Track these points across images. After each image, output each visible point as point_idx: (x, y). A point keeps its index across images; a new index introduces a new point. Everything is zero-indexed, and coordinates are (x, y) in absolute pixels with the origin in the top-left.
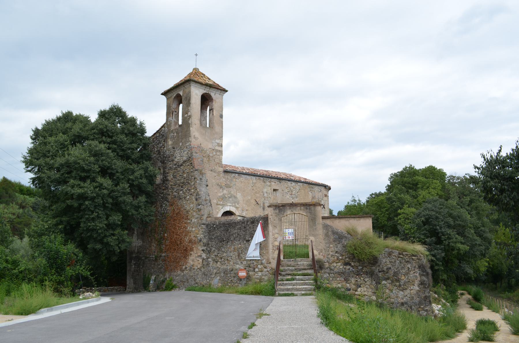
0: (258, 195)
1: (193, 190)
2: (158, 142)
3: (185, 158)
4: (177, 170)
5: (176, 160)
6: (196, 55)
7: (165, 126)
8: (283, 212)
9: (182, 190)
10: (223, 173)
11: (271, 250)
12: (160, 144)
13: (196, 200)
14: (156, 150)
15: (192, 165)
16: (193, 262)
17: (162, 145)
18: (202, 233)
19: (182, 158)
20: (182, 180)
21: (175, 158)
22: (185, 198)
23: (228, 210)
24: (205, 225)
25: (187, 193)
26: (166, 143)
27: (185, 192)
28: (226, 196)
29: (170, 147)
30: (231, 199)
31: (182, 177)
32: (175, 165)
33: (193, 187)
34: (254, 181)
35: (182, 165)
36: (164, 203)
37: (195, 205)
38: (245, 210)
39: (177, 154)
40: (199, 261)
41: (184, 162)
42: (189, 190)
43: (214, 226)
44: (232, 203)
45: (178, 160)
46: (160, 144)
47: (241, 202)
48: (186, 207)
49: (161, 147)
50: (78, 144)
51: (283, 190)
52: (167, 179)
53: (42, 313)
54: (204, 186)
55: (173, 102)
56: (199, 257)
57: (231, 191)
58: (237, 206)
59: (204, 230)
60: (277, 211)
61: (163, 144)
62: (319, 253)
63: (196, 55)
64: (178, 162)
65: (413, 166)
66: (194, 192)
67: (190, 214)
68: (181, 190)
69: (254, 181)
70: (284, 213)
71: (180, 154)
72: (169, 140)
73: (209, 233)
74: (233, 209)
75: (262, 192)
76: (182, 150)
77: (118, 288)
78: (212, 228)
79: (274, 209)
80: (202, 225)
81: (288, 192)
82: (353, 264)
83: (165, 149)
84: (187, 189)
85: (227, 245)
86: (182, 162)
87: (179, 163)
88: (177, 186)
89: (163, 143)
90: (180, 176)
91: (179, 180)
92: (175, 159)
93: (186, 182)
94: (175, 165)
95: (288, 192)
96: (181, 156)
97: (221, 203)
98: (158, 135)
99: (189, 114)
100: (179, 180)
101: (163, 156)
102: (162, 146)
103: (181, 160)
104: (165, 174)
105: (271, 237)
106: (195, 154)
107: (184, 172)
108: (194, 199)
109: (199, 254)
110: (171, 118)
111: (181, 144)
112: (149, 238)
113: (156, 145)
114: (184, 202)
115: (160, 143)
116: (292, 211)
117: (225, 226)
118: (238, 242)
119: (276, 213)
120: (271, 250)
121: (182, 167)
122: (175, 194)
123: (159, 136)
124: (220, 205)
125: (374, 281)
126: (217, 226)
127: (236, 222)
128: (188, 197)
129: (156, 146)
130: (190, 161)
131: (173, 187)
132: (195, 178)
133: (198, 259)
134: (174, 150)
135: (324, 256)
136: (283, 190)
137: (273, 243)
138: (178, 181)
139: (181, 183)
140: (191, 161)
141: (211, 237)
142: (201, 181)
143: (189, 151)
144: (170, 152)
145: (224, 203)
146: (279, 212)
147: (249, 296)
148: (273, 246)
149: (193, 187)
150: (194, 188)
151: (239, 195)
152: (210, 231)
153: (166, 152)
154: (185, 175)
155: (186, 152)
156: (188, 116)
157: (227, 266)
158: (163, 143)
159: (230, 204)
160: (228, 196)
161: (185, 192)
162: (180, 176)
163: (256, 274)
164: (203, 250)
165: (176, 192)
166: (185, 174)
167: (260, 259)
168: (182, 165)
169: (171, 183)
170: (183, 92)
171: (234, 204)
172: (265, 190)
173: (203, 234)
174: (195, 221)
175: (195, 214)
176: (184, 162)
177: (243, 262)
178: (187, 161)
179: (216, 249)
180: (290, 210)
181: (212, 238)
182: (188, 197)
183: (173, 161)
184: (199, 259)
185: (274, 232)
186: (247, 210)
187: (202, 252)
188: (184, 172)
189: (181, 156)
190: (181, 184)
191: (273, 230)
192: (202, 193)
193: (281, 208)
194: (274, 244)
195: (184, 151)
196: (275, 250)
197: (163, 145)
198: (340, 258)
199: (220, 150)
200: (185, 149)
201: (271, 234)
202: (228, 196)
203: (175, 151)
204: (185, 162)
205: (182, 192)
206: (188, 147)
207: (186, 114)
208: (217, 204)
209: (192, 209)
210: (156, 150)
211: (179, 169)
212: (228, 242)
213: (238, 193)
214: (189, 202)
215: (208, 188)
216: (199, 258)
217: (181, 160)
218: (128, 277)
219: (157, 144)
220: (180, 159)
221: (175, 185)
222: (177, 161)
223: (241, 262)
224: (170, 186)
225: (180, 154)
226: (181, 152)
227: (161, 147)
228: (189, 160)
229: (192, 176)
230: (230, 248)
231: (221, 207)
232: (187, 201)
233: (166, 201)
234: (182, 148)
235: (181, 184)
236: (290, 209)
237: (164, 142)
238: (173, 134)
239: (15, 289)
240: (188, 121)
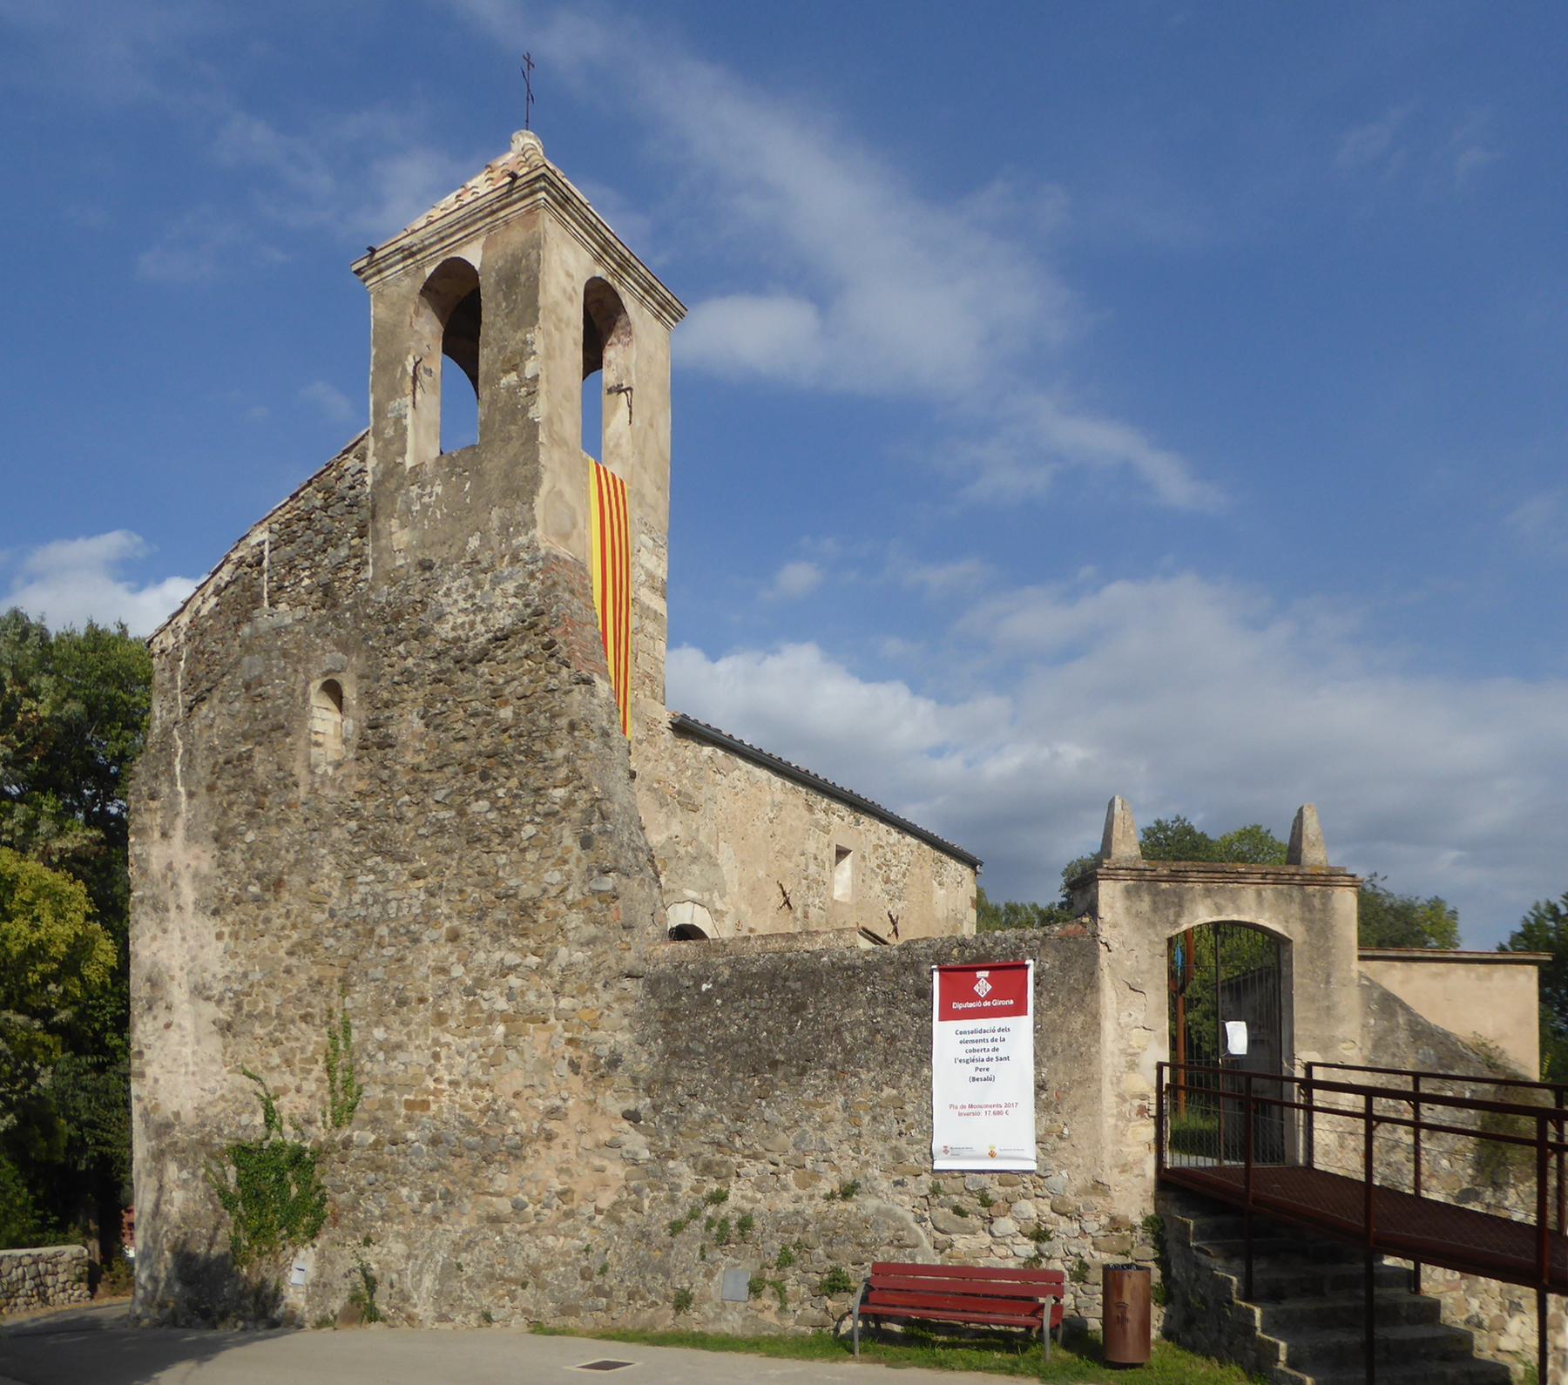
1: (559, 793)
2: (319, 539)
3: (503, 619)
4: (449, 683)
5: (445, 630)
7: (365, 448)
8: (1171, 912)
9: (488, 791)
10: (668, 734)
11: (1112, 1121)
12: (336, 546)
13: (586, 843)
15: (552, 656)
16: (565, 1178)
17: (344, 552)
18: (626, 1022)
19: (483, 621)
20: (486, 740)
21: (440, 617)
22: (507, 834)
24: (641, 982)
25: (523, 806)
26: (376, 538)
27: (508, 801)
28: (682, 851)
29: (400, 562)
30: (695, 869)
31: (486, 724)
32: (437, 657)
33: (563, 772)
34: (779, 797)
35: (483, 656)
36: (369, 863)
37: (576, 873)
39: (446, 595)
40: (601, 1170)
41: (501, 638)
42: (537, 791)
43: (705, 987)
44: (701, 890)
45: (453, 629)
46: (336, 546)
47: (733, 888)
48: (513, 882)
49: (338, 568)
51: (863, 857)
52: (387, 736)
55: (417, 313)
56: (607, 1152)
57: (698, 829)
58: (719, 906)
59: (630, 1007)
60: (1145, 905)
61: (351, 547)
64: (457, 640)
65: (1264, 829)
66: (570, 803)
67: (542, 919)
68: (478, 795)
69: (779, 797)
70: (1179, 915)
71: (472, 596)
72: (394, 522)
73: (665, 1023)
74: (702, 920)
75: (803, 854)
76: (485, 571)
77: (718, 1318)
78: (690, 997)
79: (1128, 892)
80: (627, 983)
83: (369, 572)
85: (796, 1087)
86: (482, 639)
87: (462, 649)
88: (449, 771)
89: (355, 542)
90: (475, 715)
91: (464, 739)
92: (437, 628)
93: (515, 749)
94: (437, 657)
96: (481, 609)
98: (318, 503)
99: (530, 368)
100: (464, 739)
101: (355, 615)
102: (348, 558)
103: (480, 628)
104: (514, 646)
107: (496, 694)
108: (569, 840)
109: (606, 1136)
110: (409, 400)
112: (274, 1051)
113: (307, 558)
114: (503, 859)
115: (331, 541)
116: (1219, 910)
117: (779, 983)
118: (884, 1075)
119: (1137, 915)
120: (1112, 1121)
121: (483, 668)
122: (445, 814)
123: (325, 508)
126: (720, 987)
127: (859, 962)
128: (529, 830)
129: (307, 564)
130: (543, 634)
131: (427, 777)
132: (572, 727)
133: (597, 1162)
134: (427, 575)
136: (863, 857)
137: (1119, 1080)
138: (459, 746)
139: (480, 754)
140: (546, 629)
141: (681, 1044)
143: (532, 575)
144: (406, 590)
146: (1155, 908)
147: (650, 1348)
148: (1122, 1098)
150: (567, 781)
151: (726, 855)
152: (671, 1011)
153: (371, 588)
154: (506, 713)
155: (510, 587)
156: (522, 382)
157: (798, 1199)
158: (355, 542)
160: (687, 852)
161: (508, 801)
162: (475, 715)
163: (1001, 1251)
164: (632, 1116)
165: (448, 807)
166: (506, 703)
167: (1033, 1166)
168: (483, 656)
169: (410, 758)
170: (485, 247)
173: (631, 1028)
174: (579, 956)
175: (575, 919)
176: (497, 639)
177: (909, 1179)
178: (516, 633)
179: (720, 1109)
180: (1208, 902)
181: (688, 1050)
182: (529, 830)
183: (422, 634)
184: (605, 1163)
185: (1124, 1019)
187: (625, 1124)
188: (496, 694)
189: (481, 609)
190: (480, 763)
191: (1119, 1011)
192: (617, 807)
193: (1164, 885)
194: (1123, 1086)
195: (496, 582)
196: (1129, 1121)
200: (504, 567)
201: (1108, 1027)
202: (687, 852)
203: (433, 584)
204: (506, 638)
205: (483, 804)
206: (524, 555)
207: (506, 372)
209: (553, 892)
210: (306, 582)
211: (463, 679)
212: (803, 1072)
213: (722, 844)
214: (531, 856)
216: (601, 1156)
217: (480, 628)
218: (1498, 1214)
219: (315, 553)
220: (472, 625)
221: (440, 768)
222: (451, 635)
223: (897, 1183)
224: (407, 773)
225: (472, 596)
227: (338, 568)
228: (533, 625)
229: (553, 717)
230: (817, 1105)
232: (523, 850)
233: (378, 853)
234: (484, 564)
235: (480, 763)
236: (1208, 893)
238: (423, 487)
240: (526, 409)
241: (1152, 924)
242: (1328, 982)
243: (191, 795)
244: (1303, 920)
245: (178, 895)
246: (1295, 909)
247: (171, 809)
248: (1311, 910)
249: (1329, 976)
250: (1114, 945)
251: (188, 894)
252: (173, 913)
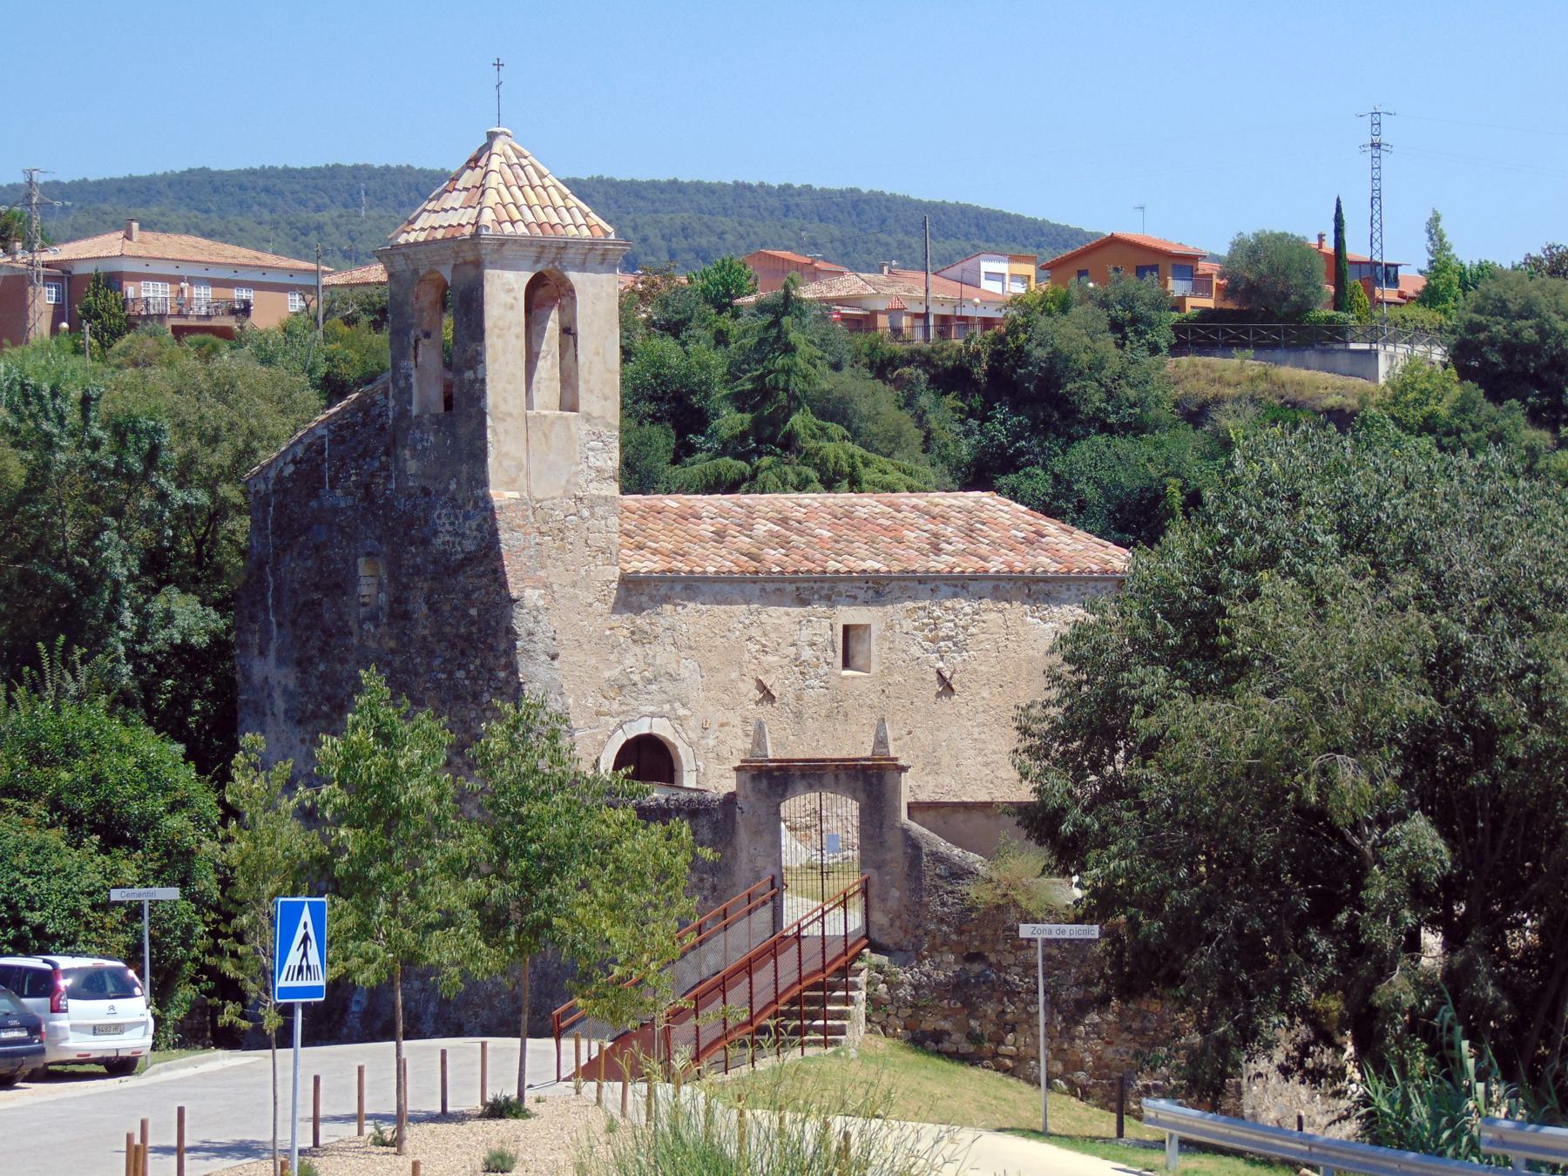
0: (772, 659)
3: (470, 545)
6: (498, 65)
14: (353, 478)
23: (645, 730)
28: (636, 678)
33: (503, 661)
38: (715, 726)
50: (200, 640)
53: (158, 1072)
54: (544, 657)
57: (654, 657)
58: (682, 712)
62: (891, 919)
63: (498, 65)
64: (445, 552)
68: (460, 666)
81: (915, 629)
82: (993, 958)
84: (482, 665)
95: (915, 629)
97: (615, 706)
105: (743, 867)
106: (507, 536)
111: (453, 486)
124: (609, 714)
125: (1059, 1012)
135: (906, 932)
142: (531, 641)
145: (624, 708)
146: (770, 787)
149: (503, 661)
159: (652, 709)
171: (667, 707)
172: (806, 634)
180: (804, 782)
183: (425, 542)
186: (722, 725)
195: (467, 517)
197: (384, 467)
198: (954, 937)
199: (606, 498)
201: (743, 857)
203: (431, 507)
208: (598, 714)
210: (353, 478)
215: (556, 663)
226: (456, 517)
231: (613, 722)
237: (387, 453)
239: (1110, 948)
241: (768, 796)
242: (881, 827)
243: (280, 625)
244: (865, 791)
245: (272, 704)
246: (860, 784)
247: (266, 632)
248: (871, 784)
249: (882, 824)
250: (745, 809)
251: (280, 705)
252: (269, 719)
